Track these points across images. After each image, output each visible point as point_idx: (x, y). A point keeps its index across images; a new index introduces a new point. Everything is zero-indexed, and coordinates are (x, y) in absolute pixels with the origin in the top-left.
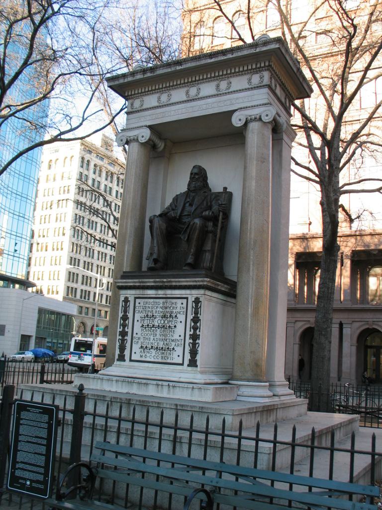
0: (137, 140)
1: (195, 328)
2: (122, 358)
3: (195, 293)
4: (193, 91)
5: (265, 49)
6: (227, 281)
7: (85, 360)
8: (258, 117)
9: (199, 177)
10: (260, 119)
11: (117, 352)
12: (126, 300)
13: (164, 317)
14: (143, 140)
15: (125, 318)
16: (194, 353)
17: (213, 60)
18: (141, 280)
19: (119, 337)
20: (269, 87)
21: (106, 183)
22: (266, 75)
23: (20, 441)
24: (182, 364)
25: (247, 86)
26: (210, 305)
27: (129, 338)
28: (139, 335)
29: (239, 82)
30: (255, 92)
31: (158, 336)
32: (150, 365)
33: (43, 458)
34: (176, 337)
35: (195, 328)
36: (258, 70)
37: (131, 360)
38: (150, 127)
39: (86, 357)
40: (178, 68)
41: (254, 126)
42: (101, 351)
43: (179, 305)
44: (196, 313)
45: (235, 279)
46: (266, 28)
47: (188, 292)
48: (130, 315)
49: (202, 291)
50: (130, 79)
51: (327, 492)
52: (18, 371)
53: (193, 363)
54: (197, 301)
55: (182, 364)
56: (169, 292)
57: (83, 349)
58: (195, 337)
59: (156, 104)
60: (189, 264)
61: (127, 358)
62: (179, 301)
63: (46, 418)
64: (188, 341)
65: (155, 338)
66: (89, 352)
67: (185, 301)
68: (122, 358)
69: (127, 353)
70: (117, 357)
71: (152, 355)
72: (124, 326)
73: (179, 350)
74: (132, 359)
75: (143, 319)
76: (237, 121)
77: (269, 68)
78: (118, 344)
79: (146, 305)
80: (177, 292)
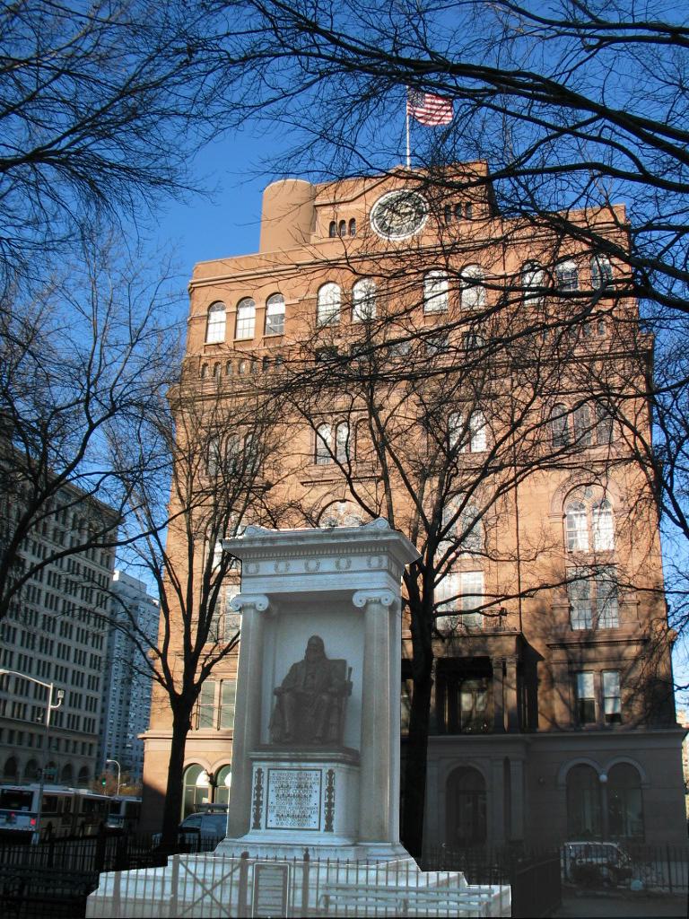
0: (254, 607)
1: (330, 797)
2: (257, 826)
3: (329, 766)
4: (312, 565)
5: (385, 538)
6: (348, 751)
7: (18, 822)
9: (316, 646)
10: (380, 602)
11: (252, 821)
12: (259, 771)
13: (299, 787)
14: (261, 609)
15: (259, 788)
16: (329, 819)
17: (335, 541)
19: (253, 807)
20: (389, 571)
21: (57, 524)
22: (385, 558)
24: (319, 830)
25: (367, 568)
26: (340, 772)
27: (263, 807)
28: (274, 804)
29: (358, 563)
30: (375, 574)
31: (294, 805)
32: (287, 832)
34: (312, 805)
35: (330, 797)
36: (376, 554)
37: (267, 828)
39: (20, 817)
40: (300, 543)
41: (374, 607)
42: (44, 808)
43: (313, 777)
44: (330, 783)
45: (357, 747)
46: (305, 241)
47: (322, 764)
48: (264, 785)
49: (335, 765)
50: (247, 545)
53: (329, 828)
54: (331, 773)
55: (319, 830)
56: (303, 765)
57: (16, 805)
58: (330, 805)
59: (274, 572)
61: (263, 825)
62: (314, 772)
63: (281, 872)
64: (324, 808)
65: (291, 807)
66: (25, 810)
67: (319, 773)
68: (257, 826)
69: (262, 821)
70: (252, 825)
71: (288, 823)
72: (258, 795)
73: (315, 817)
74: (269, 826)
75: (277, 789)
76: (358, 601)
77: (388, 553)
78: (252, 813)
79: (277, 779)
80: (311, 765)
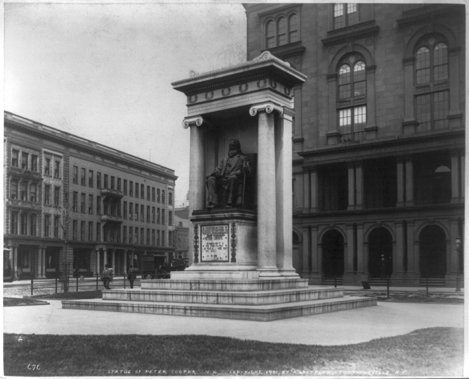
8: (264, 110)
11: (194, 258)
18: (246, 70)
23: (173, 297)
24: (228, 261)
27: (199, 249)
33: (344, 26)
38: (203, 116)
41: (263, 118)
51: (54, 273)
52: (220, 285)
60: (229, 204)
61: (199, 260)
68: (196, 261)
70: (194, 260)
